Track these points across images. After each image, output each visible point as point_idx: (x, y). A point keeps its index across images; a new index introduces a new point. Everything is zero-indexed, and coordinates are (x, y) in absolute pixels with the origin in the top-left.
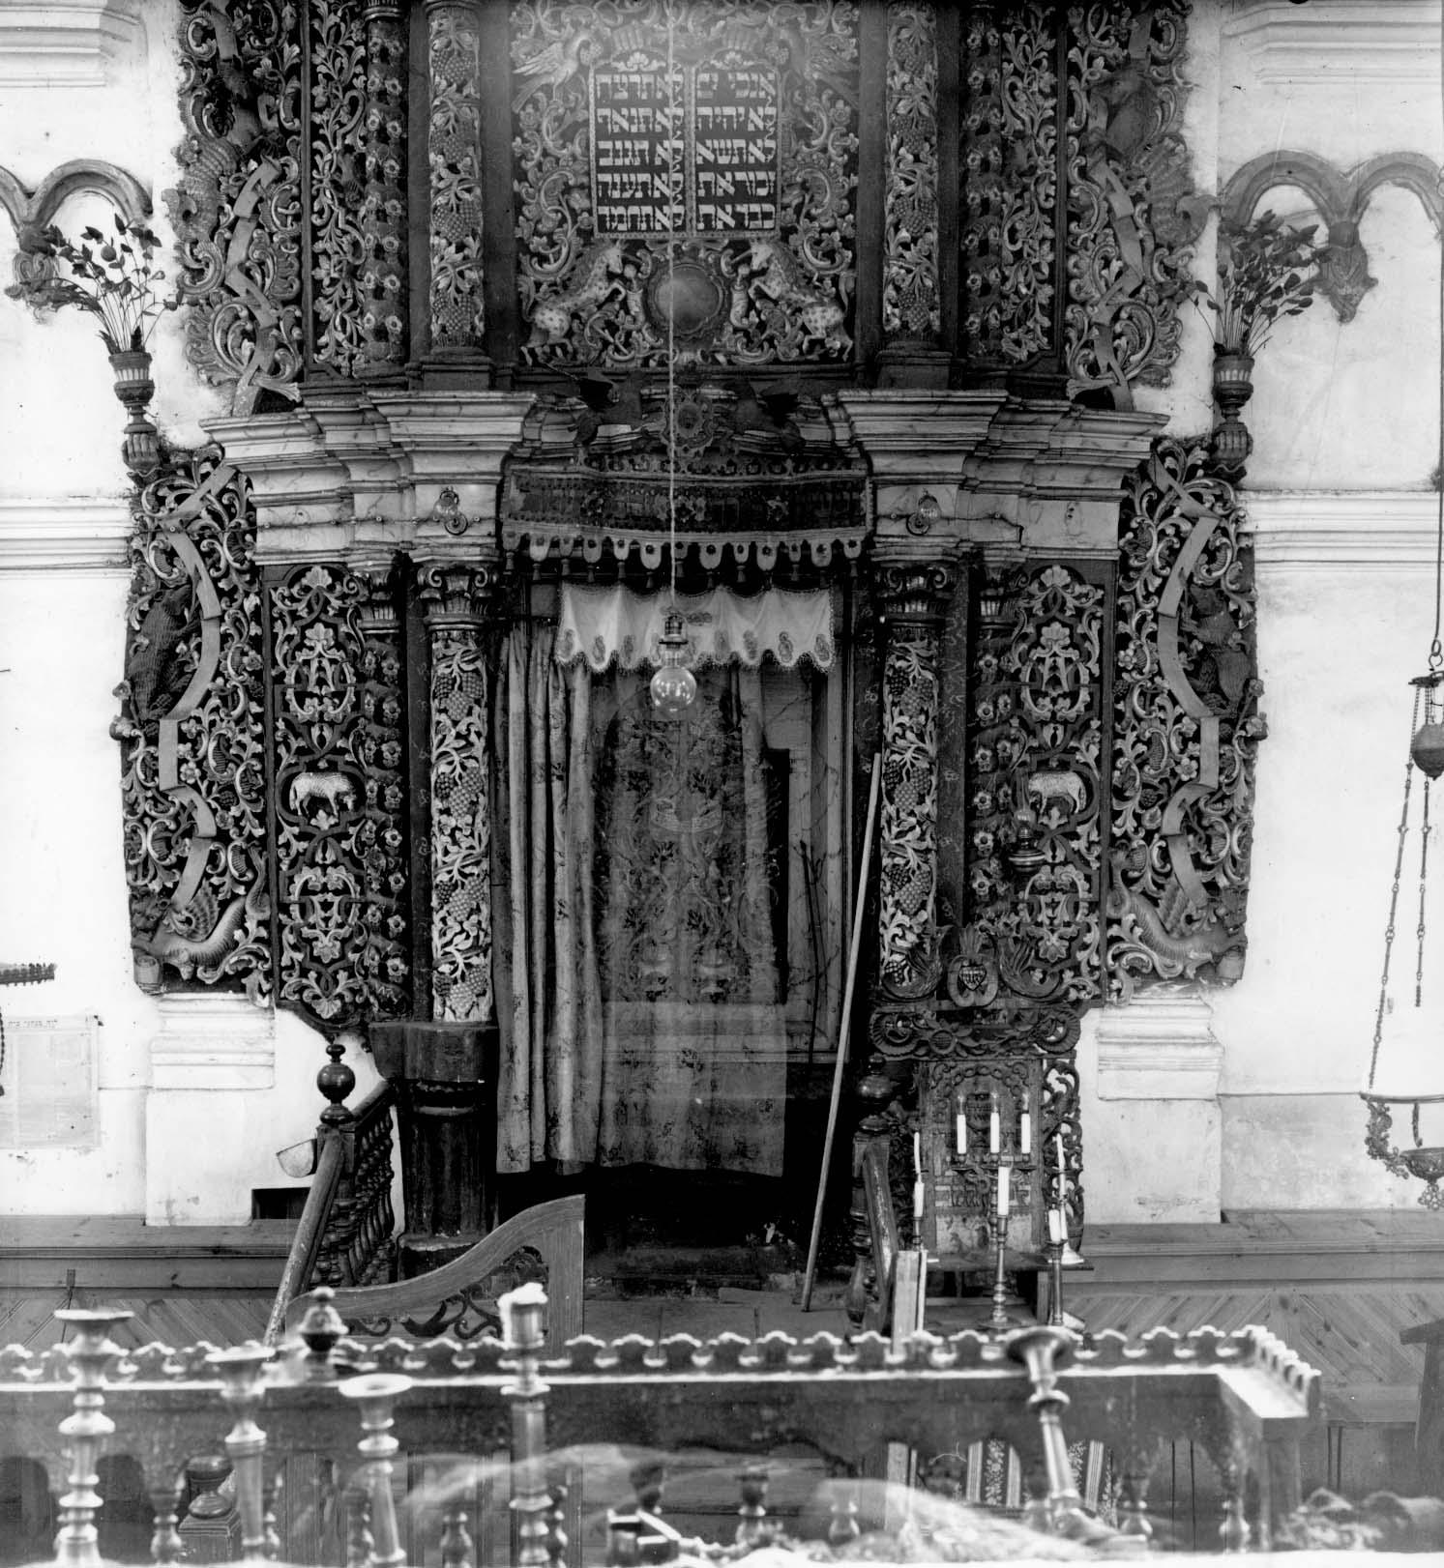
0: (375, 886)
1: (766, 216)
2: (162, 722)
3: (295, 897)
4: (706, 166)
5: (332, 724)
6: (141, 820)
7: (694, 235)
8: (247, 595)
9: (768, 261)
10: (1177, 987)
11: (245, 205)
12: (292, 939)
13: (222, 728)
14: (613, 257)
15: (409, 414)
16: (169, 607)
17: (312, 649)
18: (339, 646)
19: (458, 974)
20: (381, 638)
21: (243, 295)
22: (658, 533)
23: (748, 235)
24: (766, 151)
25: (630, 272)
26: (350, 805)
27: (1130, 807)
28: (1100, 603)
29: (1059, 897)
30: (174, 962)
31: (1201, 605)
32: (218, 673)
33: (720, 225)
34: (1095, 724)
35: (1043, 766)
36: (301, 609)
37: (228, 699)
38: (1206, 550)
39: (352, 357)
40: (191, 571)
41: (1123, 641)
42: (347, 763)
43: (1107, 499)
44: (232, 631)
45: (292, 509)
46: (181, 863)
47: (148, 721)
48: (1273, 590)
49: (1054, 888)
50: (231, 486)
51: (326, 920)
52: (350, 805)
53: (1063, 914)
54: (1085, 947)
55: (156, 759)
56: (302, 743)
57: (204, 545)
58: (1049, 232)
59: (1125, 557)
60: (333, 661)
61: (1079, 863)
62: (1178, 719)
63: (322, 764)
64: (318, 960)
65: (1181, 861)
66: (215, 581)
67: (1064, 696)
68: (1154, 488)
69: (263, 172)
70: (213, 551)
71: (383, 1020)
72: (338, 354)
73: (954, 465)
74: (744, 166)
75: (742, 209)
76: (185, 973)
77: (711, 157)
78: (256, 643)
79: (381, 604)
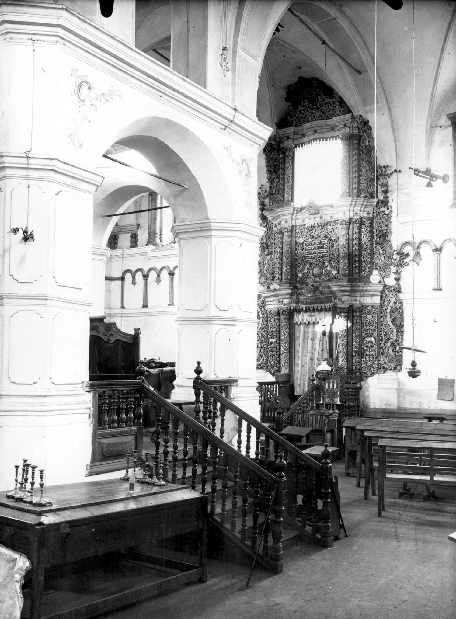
4: (319, 253)
7: (318, 262)
11: (266, 262)
13: (262, 333)
14: (308, 266)
25: (310, 268)
27: (383, 342)
28: (377, 311)
29: (370, 356)
31: (394, 311)
35: (368, 336)
37: (263, 328)
38: (394, 302)
41: (382, 317)
43: (378, 296)
49: (369, 355)
53: (371, 359)
54: (375, 364)
58: (370, 257)
59: (381, 304)
62: (390, 329)
65: (391, 350)
69: (269, 257)
73: (347, 293)
74: (323, 253)
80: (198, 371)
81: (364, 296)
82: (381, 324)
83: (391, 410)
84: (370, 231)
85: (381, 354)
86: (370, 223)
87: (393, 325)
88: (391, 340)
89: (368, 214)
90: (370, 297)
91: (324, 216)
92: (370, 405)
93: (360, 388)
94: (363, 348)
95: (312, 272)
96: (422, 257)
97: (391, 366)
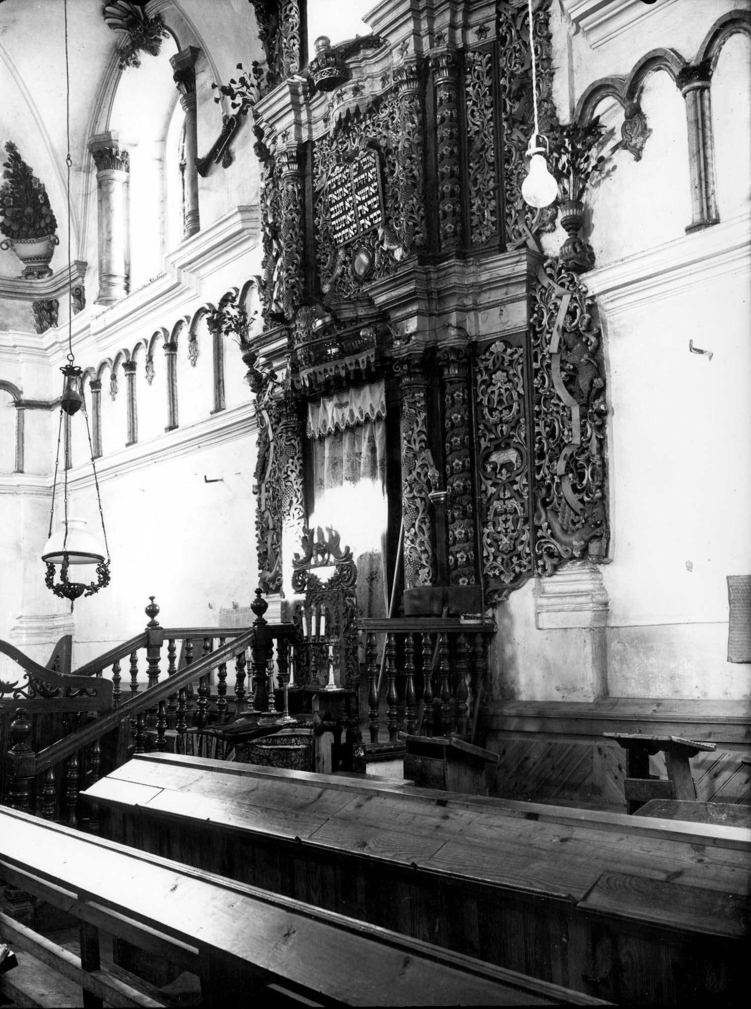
10: (579, 563)
27: (546, 462)
34: (522, 420)
35: (498, 448)
48: (616, 325)
49: (506, 512)
58: (493, 174)
61: (517, 497)
67: (505, 409)
68: (543, 287)
74: (370, 198)
80: (152, 611)
81: (476, 308)
82: (535, 396)
83: (575, 709)
84: (490, 87)
85: (539, 504)
86: (490, 59)
87: (571, 392)
88: (567, 451)
89: (482, 31)
90: (496, 310)
91: (366, 84)
92: (519, 693)
93: (488, 633)
94: (485, 492)
96: (650, 124)
97: (570, 544)
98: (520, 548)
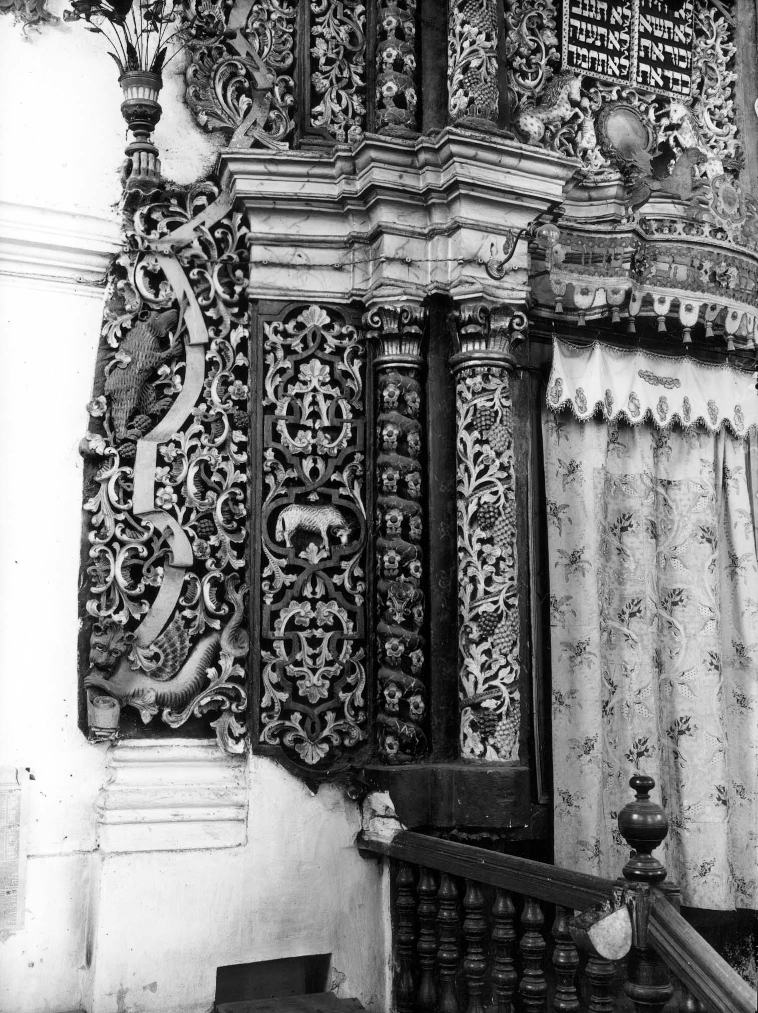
0: (398, 618)
1: (685, 84)
2: (140, 442)
3: (280, 632)
5: (326, 457)
6: (109, 545)
7: (635, 82)
8: (234, 326)
9: (682, 119)
12: (275, 677)
13: (204, 454)
14: (575, 86)
15: (474, 158)
16: (153, 328)
17: (305, 383)
18: (334, 383)
19: (504, 709)
20: (403, 371)
21: (244, 56)
22: (699, 294)
23: (671, 95)
24: (686, 35)
26: (344, 540)
30: (137, 703)
32: (201, 400)
33: (653, 83)
36: (297, 345)
39: (347, 128)
40: (180, 297)
42: (341, 496)
44: (218, 359)
45: (291, 250)
46: (151, 593)
47: (125, 440)
50: (225, 222)
51: (314, 657)
52: (344, 540)
55: (131, 481)
56: (294, 474)
57: (194, 274)
60: (327, 397)
63: (313, 497)
64: (304, 700)
66: (204, 309)
70: (202, 278)
71: (401, 763)
72: (333, 122)
75: (669, 74)
76: (146, 718)
77: (650, 29)
78: (241, 373)
79: (411, 337)
95: (601, 139)
98: (288, 364)
